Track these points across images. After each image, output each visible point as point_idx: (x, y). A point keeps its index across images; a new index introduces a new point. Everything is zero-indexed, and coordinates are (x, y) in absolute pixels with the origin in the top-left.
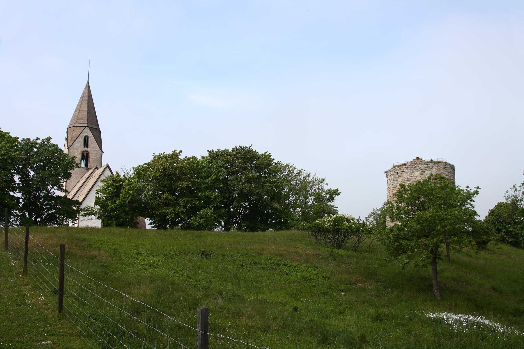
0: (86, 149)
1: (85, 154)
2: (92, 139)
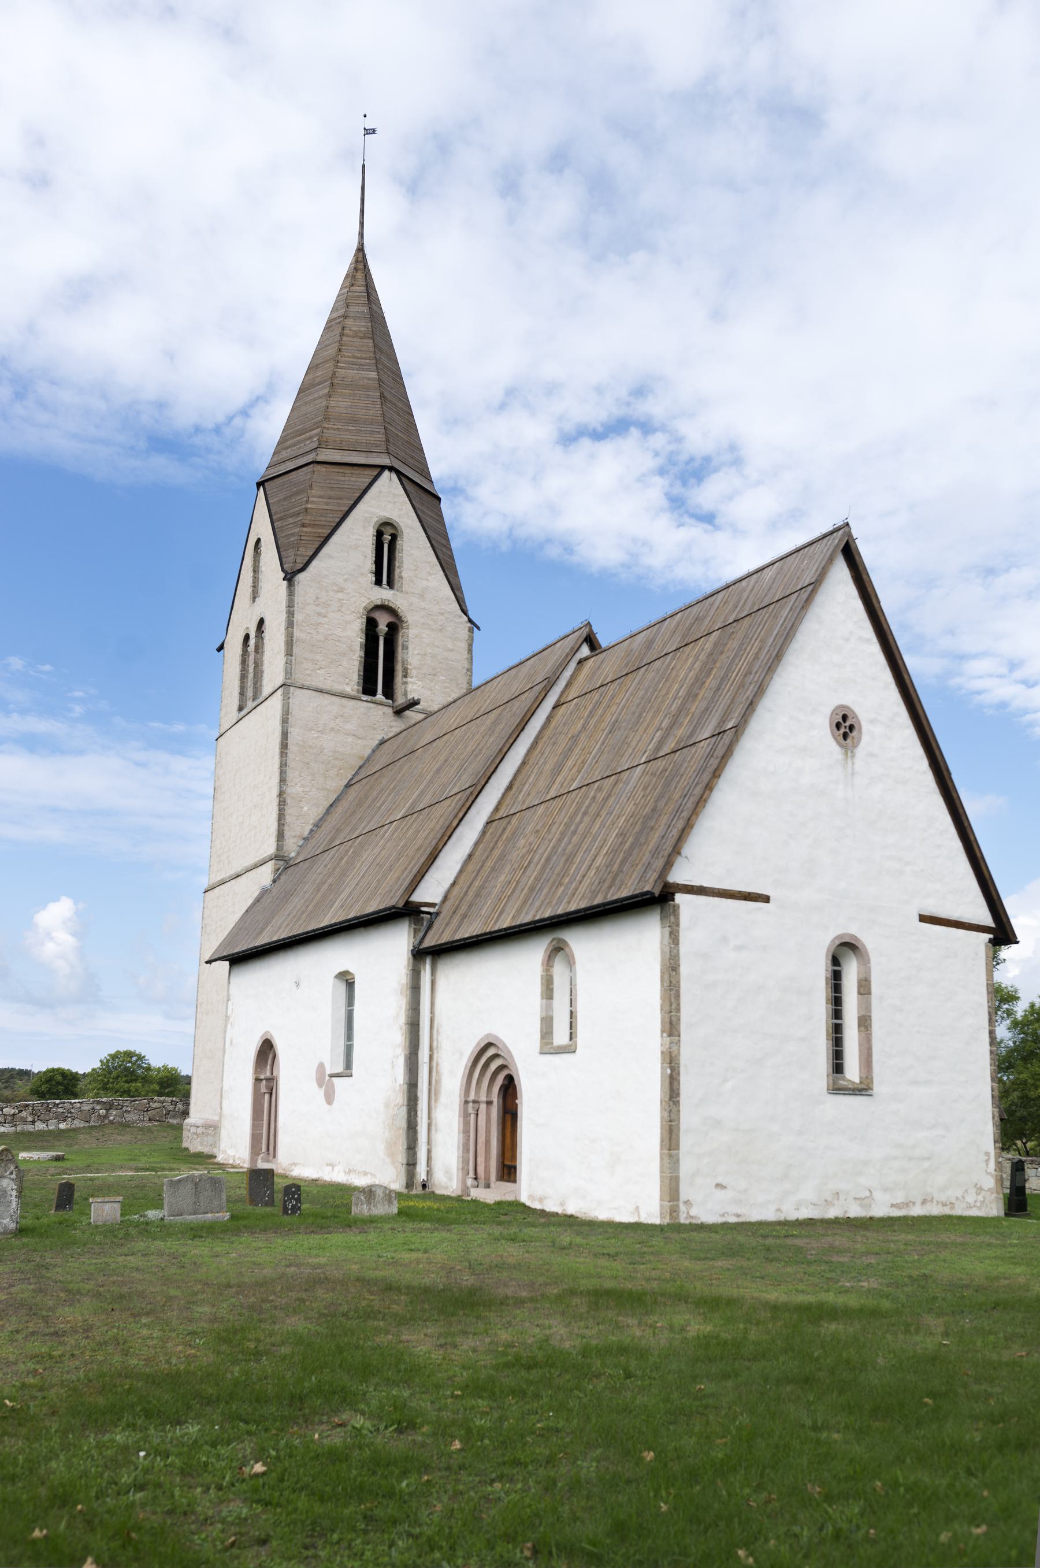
0: (383, 595)
1: (382, 628)
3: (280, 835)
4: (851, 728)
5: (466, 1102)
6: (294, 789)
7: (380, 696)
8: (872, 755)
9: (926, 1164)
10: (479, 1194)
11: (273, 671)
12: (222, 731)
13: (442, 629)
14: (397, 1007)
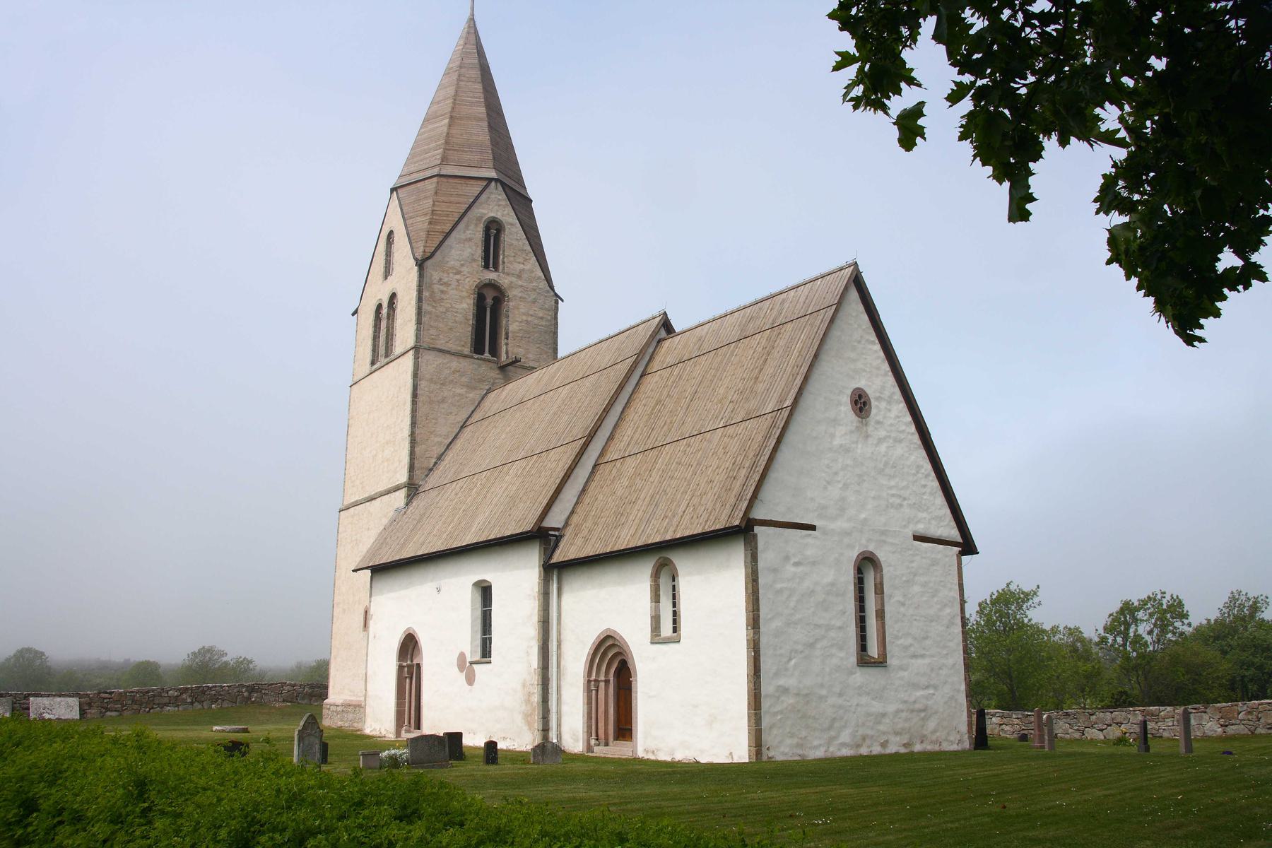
0: (491, 276)
1: (489, 301)
4: (865, 404)
5: (589, 681)
7: (487, 355)
8: (878, 422)
9: (923, 715)
10: (600, 751)
11: (405, 334)
12: (356, 379)
13: (534, 302)
14: (531, 608)
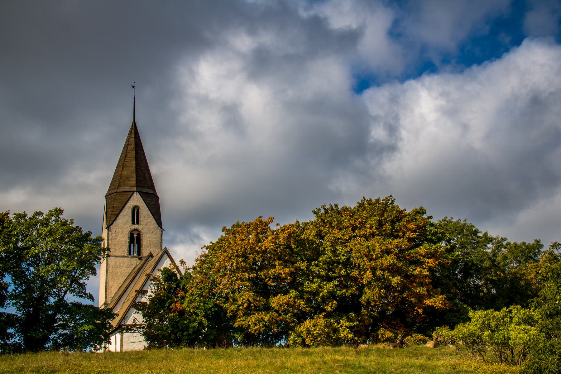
0: (136, 226)
1: (135, 236)
2: (145, 211)
3: (106, 298)
6: (110, 284)
